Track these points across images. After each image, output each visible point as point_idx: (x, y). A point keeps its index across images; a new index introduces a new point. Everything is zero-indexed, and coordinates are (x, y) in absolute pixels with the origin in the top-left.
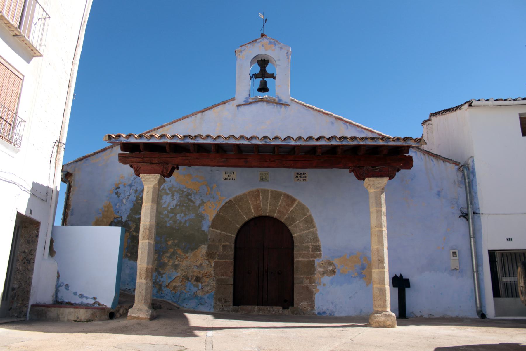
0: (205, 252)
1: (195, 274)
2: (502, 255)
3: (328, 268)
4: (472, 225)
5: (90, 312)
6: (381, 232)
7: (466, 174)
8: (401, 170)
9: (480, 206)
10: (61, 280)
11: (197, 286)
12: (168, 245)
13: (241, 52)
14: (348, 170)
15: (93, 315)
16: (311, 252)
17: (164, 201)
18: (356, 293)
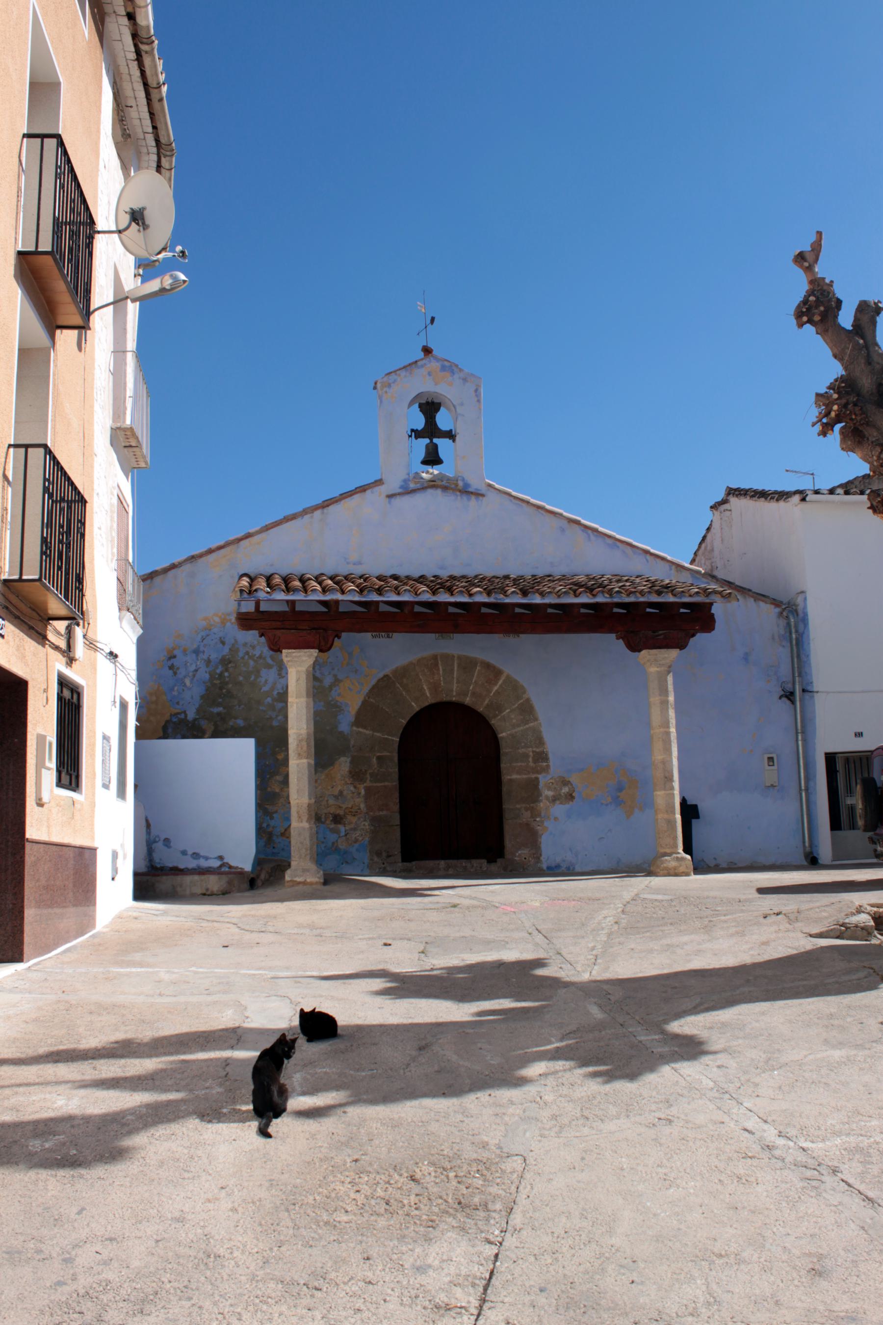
0: (347, 769)
1: (332, 810)
2: (847, 760)
3: (561, 789)
4: (801, 712)
5: (225, 879)
6: (668, 734)
7: (792, 624)
8: (698, 635)
9: (814, 680)
10: (154, 832)
11: (338, 832)
12: (278, 760)
13: (389, 386)
14: (613, 636)
15: (230, 883)
16: (531, 764)
17: (263, 680)
18: (610, 830)
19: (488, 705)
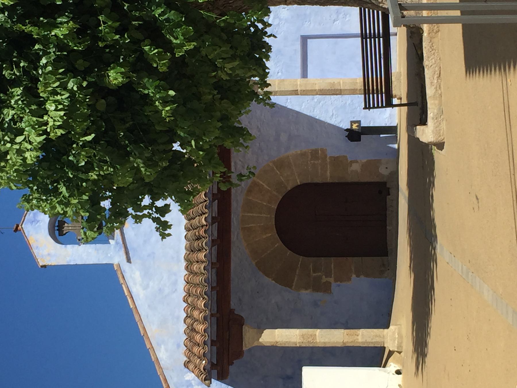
19: (277, 192)
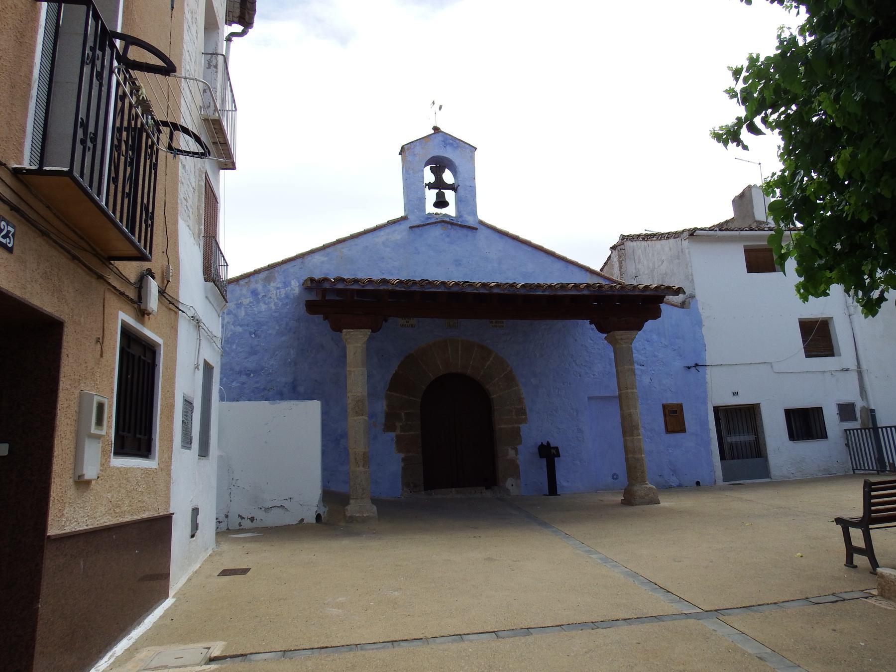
16: (515, 417)
